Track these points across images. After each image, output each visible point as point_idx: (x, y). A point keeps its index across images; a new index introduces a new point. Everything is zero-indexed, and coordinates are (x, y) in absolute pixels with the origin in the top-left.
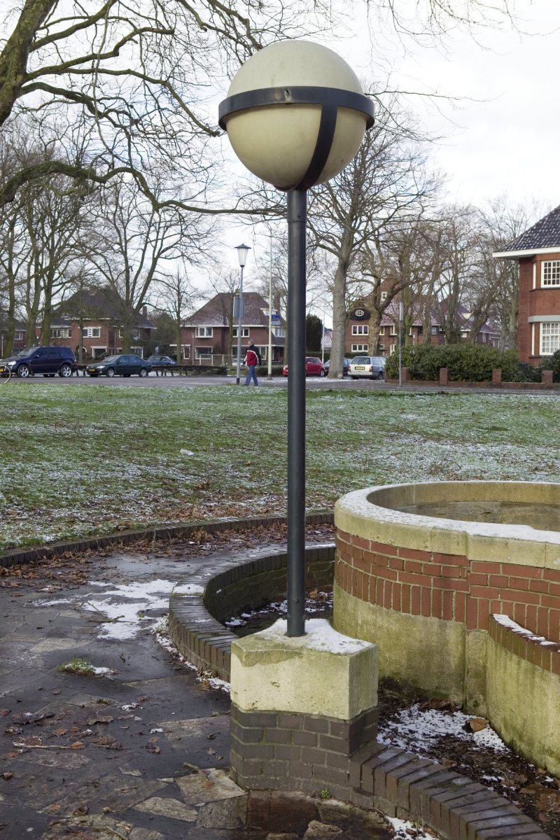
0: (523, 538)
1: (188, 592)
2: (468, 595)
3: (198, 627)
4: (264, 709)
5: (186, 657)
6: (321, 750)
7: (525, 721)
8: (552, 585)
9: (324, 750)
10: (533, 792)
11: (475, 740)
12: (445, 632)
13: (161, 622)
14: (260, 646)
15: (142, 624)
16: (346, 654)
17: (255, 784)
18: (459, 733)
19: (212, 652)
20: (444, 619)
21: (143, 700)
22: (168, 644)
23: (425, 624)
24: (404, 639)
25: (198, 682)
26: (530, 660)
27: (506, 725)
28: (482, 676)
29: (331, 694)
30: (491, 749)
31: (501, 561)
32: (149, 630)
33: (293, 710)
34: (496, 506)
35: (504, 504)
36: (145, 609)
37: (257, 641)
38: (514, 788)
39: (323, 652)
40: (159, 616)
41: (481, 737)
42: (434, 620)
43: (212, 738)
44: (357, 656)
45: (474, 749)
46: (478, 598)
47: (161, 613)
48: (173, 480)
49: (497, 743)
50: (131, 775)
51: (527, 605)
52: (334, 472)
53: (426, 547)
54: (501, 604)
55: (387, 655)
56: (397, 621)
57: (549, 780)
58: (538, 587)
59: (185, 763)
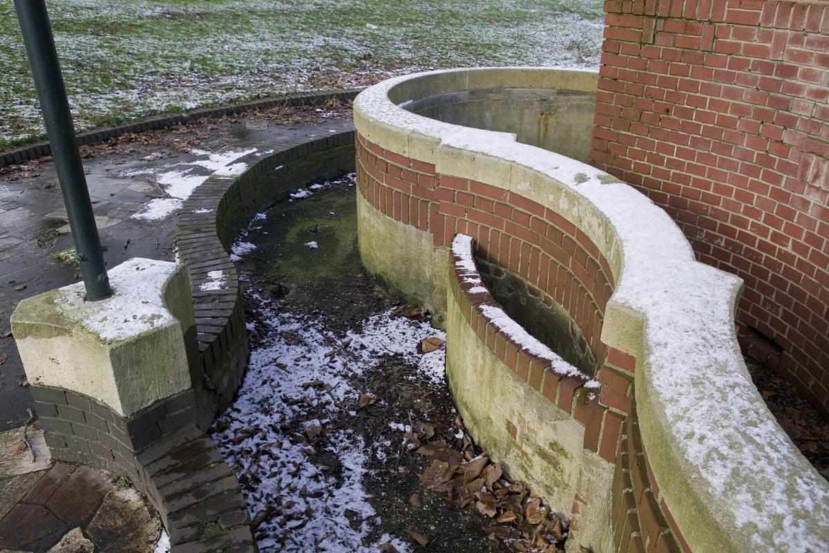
0: (493, 153)
18: (410, 353)
20: (421, 229)
23: (405, 231)
31: (468, 177)
34: (552, 94)
35: (560, 92)
41: (428, 361)
44: (128, 344)
48: (346, 51)
52: (483, 46)
53: (404, 152)
58: (504, 209)
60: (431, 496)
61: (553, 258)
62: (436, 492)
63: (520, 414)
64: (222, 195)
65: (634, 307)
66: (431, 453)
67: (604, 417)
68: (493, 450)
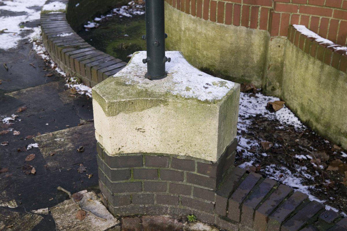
1: (54, 9)
2: (271, 10)
3: (63, 42)
4: (130, 152)
5: (56, 64)
6: (188, 184)
9: (190, 184)
10: (336, 169)
11: (278, 118)
12: (251, 37)
13: (37, 33)
14: (122, 94)
15: (22, 35)
16: (214, 102)
17: (125, 212)
19: (76, 64)
21: (22, 111)
22: (41, 52)
23: (236, 31)
24: (218, 42)
25: (66, 88)
26: (335, 65)
28: (280, 70)
29: (198, 138)
30: (291, 126)
32: (27, 40)
33: (159, 152)
36: (25, 21)
37: (119, 87)
38: (321, 167)
39: (189, 99)
40: (35, 27)
41: (282, 116)
42: (243, 29)
43: (82, 151)
45: (280, 127)
46: (281, 13)
47: (36, 24)
49: (293, 120)
50: (7, 208)
51: (321, 17)
54: (300, 17)
55: (205, 53)
56: (214, 29)
59: (59, 188)
66: (336, 169)
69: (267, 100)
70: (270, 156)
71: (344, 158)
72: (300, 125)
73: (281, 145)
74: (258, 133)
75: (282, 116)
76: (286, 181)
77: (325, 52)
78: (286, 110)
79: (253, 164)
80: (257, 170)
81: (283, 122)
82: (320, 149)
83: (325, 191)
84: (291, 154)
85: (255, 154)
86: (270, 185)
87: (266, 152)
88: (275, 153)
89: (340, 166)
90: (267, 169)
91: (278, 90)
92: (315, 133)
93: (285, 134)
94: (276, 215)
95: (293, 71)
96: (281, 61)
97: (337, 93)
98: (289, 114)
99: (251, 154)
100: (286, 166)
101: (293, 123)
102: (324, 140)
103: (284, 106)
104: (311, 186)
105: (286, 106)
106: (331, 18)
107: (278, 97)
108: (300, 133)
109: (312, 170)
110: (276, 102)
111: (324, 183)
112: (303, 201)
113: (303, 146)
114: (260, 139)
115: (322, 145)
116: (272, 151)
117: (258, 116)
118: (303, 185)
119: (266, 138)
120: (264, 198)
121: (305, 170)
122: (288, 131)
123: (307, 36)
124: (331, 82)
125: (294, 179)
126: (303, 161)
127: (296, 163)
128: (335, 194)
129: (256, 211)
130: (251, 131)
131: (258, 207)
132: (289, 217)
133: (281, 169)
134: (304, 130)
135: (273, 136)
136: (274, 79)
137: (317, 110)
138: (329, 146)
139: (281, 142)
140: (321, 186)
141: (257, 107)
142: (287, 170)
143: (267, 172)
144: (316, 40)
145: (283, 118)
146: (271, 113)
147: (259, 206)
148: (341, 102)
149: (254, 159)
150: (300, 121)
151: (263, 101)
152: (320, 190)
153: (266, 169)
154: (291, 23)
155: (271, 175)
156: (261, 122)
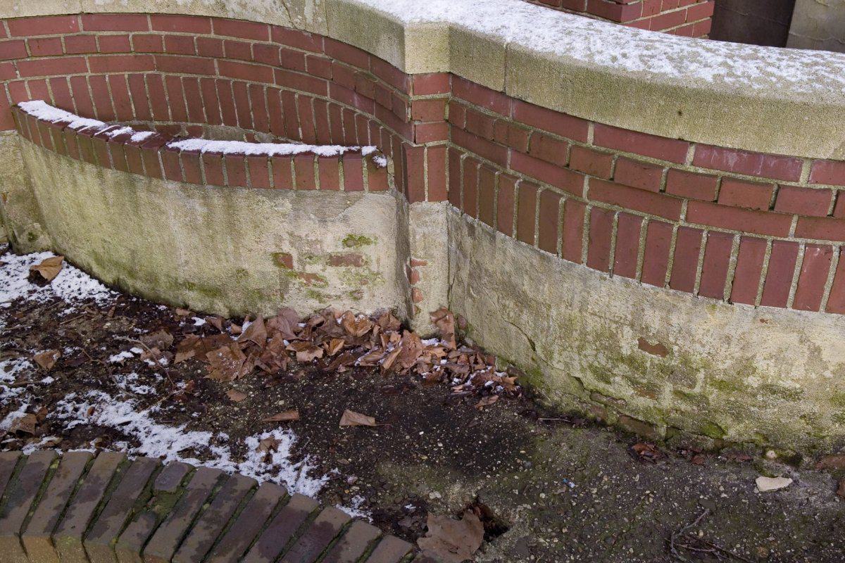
7: (133, 252)
8: (101, 37)
10: (191, 354)
11: (59, 294)
26: (120, 166)
27: (99, 261)
38: (164, 361)
41: (66, 287)
45: (68, 311)
49: (90, 287)
51: (68, 77)
57: (200, 322)
58: (79, 46)
60: (243, 383)
61: (182, 76)
62: (244, 377)
63: (291, 234)
64: (105, 12)
65: (432, 20)
66: (191, 354)
67: (426, 156)
68: (259, 305)
69: (27, 262)
70: (59, 380)
71: (199, 328)
72: (105, 292)
73: (76, 348)
74: (24, 339)
75: (66, 287)
76: (103, 417)
77: (93, 146)
78: (70, 272)
79: (29, 411)
80: (38, 419)
81: (71, 297)
82: (154, 327)
83: (181, 407)
84: (101, 359)
85: (28, 385)
86: (43, 464)
87: (51, 374)
88: (69, 368)
89: (196, 345)
90: (61, 409)
91: (42, 237)
92: (138, 298)
93: (81, 320)
94: (68, 524)
95: (53, 194)
96: (25, 179)
97: (145, 215)
98: (79, 276)
99: (19, 390)
100: (96, 386)
101: (92, 294)
102: (157, 306)
103: (66, 265)
104: (153, 408)
105: (68, 263)
106: (88, 74)
107: (48, 250)
108: (108, 309)
109: (147, 373)
110: (45, 263)
111: (175, 392)
112: (117, 468)
113: (121, 333)
114: (32, 351)
115: (156, 317)
116: (62, 366)
117: (16, 303)
118: (139, 411)
119: (44, 344)
120: (35, 500)
121: (136, 380)
122: (86, 312)
123: (50, 122)
124: (126, 199)
125: (118, 408)
126: (128, 364)
127: (115, 372)
128: (200, 403)
129: (23, 536)
130: (8, 341)
131: (27, 526)
132: (95, 516)
133: (88, 398)
134: (116, 299)
135: (57, 334)
136: (26, 218)
137: (123, 255)
138: (168, 314)
139: (75, 340)
140: (172, 399)
141: (8, 285)
142: (100, 393)
143: (61, 416)
144: (70, 126)
145: (68, 291)
146: (42, 289)
147: (27, 520)
148: (158, 231)
149: (29, 397)
150: (103, 285)
151: (20, 269)
152: (171, 407)
153: (59, 409)
154: (13, 101)
155: (71, 418)
156: (25, 313)
